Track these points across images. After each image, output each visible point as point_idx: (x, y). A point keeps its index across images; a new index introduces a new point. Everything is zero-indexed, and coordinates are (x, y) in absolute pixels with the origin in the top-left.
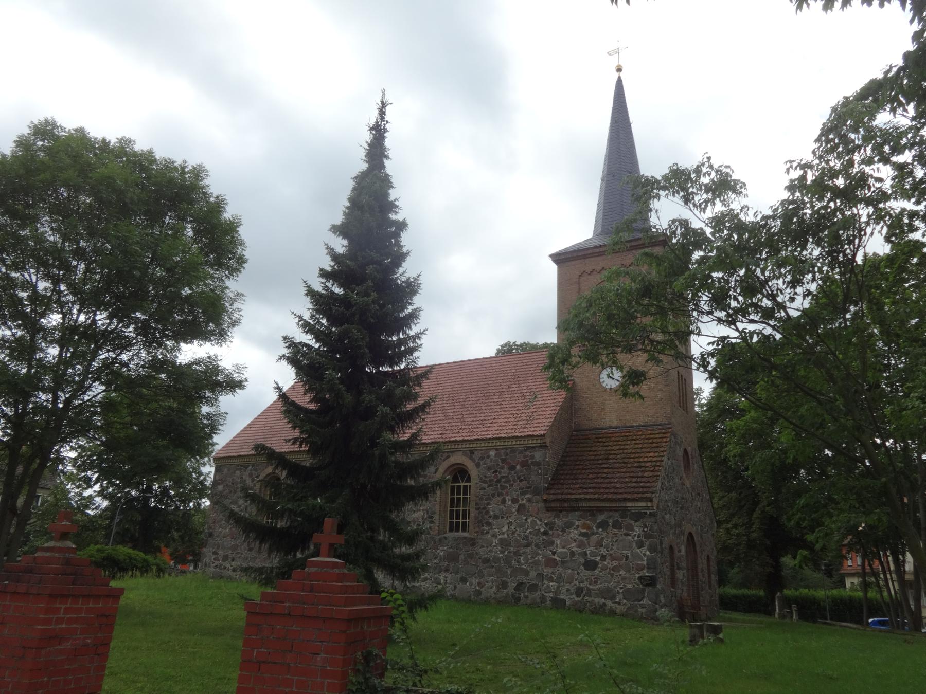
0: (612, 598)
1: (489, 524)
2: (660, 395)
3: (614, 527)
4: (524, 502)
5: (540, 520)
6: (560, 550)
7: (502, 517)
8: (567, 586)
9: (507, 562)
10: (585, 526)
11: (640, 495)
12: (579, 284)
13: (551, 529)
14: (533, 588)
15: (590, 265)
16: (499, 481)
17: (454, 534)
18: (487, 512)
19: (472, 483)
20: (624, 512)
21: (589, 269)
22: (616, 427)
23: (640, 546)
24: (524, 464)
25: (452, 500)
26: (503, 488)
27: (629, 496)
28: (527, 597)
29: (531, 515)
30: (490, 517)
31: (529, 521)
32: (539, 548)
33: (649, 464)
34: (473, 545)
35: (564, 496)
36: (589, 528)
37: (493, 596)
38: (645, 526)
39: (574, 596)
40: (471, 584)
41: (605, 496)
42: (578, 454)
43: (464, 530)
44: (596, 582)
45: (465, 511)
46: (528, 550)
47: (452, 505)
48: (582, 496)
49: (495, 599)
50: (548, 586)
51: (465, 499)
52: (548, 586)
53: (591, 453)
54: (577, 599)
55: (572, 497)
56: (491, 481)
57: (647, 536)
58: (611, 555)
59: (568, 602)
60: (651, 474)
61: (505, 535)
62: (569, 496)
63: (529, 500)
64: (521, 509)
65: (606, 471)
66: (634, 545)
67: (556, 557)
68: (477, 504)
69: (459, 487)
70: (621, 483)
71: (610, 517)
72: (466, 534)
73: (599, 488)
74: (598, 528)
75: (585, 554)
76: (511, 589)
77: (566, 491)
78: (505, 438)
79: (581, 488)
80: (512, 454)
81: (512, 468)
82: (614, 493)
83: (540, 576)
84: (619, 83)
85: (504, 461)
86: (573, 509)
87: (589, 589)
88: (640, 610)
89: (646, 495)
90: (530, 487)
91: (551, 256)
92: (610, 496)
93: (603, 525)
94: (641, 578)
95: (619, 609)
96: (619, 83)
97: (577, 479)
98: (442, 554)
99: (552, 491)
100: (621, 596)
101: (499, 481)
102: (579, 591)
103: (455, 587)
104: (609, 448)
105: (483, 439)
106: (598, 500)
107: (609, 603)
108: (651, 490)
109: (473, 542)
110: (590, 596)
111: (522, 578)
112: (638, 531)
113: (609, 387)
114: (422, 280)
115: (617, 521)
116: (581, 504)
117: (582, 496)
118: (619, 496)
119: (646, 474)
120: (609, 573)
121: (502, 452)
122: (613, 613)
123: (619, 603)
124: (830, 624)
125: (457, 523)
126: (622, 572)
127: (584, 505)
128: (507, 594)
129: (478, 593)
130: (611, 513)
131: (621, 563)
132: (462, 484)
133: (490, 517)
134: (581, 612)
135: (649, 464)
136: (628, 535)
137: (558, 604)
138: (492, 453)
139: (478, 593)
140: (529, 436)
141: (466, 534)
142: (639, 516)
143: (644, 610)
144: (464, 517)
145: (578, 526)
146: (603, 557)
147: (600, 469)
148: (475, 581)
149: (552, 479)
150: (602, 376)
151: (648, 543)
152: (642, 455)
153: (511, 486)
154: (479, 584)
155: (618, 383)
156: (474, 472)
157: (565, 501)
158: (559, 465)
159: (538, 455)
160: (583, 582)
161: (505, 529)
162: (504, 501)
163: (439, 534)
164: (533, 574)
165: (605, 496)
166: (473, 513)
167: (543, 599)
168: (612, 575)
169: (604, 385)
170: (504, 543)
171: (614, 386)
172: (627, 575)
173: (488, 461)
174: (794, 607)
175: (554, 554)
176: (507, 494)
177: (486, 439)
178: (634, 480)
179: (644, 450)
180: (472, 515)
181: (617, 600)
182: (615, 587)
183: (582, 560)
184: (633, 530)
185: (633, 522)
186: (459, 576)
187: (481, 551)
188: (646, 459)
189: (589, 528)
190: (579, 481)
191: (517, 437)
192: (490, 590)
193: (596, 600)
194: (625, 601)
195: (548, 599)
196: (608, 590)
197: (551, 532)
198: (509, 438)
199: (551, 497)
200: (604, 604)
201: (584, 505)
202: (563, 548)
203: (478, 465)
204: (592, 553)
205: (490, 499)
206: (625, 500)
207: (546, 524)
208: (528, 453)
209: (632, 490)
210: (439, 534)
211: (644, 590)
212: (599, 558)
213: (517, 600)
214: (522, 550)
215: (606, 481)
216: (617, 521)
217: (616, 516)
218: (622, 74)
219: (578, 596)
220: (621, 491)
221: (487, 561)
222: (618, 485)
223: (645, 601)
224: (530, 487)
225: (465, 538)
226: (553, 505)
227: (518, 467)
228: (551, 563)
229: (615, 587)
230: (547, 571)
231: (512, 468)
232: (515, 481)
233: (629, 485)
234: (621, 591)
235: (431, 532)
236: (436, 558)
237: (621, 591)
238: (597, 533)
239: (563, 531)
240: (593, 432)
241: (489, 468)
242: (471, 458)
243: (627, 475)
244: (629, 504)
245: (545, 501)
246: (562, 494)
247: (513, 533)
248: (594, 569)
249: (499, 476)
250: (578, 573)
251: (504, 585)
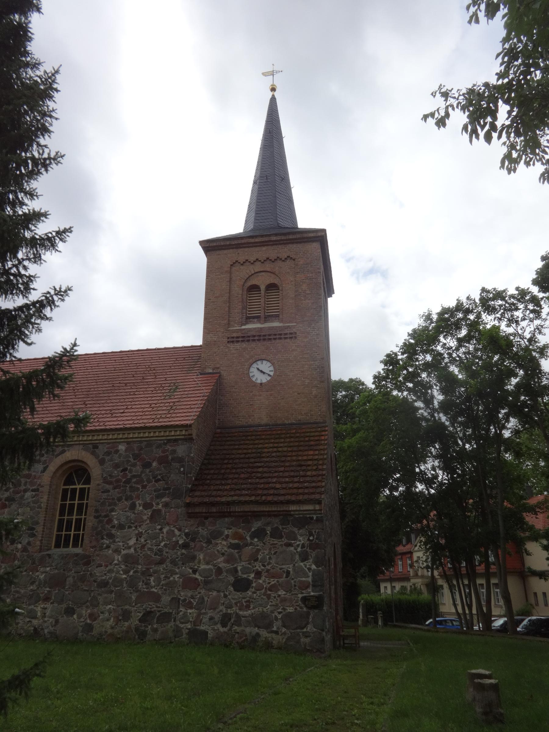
0: (268, 627)
1: (111, 536)
2: (314, 392)
3: (272, 536)
4: (160, 507)
5: (180, 530)
6: (203, 567)
7: (130, 527)
8: (211, 613)
9: (132, 584)
10: (236, 536)
11: (306, 497)
12: (230, 273)
13: (193, 540)
14: (165, 617)
15: (242, 255)
16: (128, 481)
17: (63, 550)
18: (110, 521)
19: (92, 486)
20: (286, 517)
21: (241, 259)
22: (266, 425)
23: (304, 558)
24: (163, 461)
25: (63, 507)
26: (133, 489)
27: (293, 498)
28: (155, 630)
29: (168, 524)
30: (113, 527)
31: (165, 530)
32: (175, 565)
33: (310, 463)
34: (88, 563)
35: (212, 499)
36: (241, 538)
37: (110, 631)
38: (311, 534)
39: (219, 626)
40: (80, 617)
41: (264, 498)
42: (225, 452)
43: (75, 545)
44: (248, 607)
45: (78, 521)
46: (161, 568)
47: (62, 513)
48: (235, 498)
49: (112, 635)
50: (185, 614)
51: (80, 506)
52: (185, 614)
53: (240, 451)
54: (222, 630)
55: (224, 499)
56: (118, 481)
57: (313, 546)
58: (268, 571)
59: (211, 635)
60: (314, 473)
61: (132, 550)
62: (218, 499)
63: (166, 505)
64: (155, 516)
65: (260, 470)
66: (297, 557)
67: (197, 576)
68: (97, 511)
69: (74, 491)
70: (280, 483)
71: (268, 524)
72: (78, 550)
73: (255, 489)
74: (252, 537)
75: (236, 570)
76: (134, 621)
77: (214, 493)
78: (141, 428)
79: (232, 489)
80: (149, 447)
81: (147, 465)
82: (274, 495)
83: (176, 601)
84: (273, 101)
85: (136, 457)
86: (223, 515)
87: (238, 616)
88: (303, 640)
89: (313, 497)
90: (168, 489)
91: (202, 243)
92: (270, 498)
93: (260, 534)
94: (304, 599)
95: (276, 640)
96: (273, 101)
97: (226, 479)
98: (42, 577)
99: (198, 493)
100: (279, 623)
101: (128, 481)
102: (225, 620)
103: (57, 622)
104: (260, 446)
105: (111, 430)
106: (257, 503)
107: (264, 633)
108: (319, 490)
109: (87, 560)
110: (239, 625)
111: (151, 606)
112: (302, 540)
113: (259, 381)
114: (61, 82)
115: (277, 528)
116: (233, 509)
117: (235, 498)
118: (281, 498)
119: (309, 473)
120: (265, 594)
121: (135, 446)
122: (268, 646)
123: (276, 633)
124: (395, 626)
125: (67, 537)
126: (282, 592)
127: (238, 509)
128: (129, 627)
129: (89, 628)
130: (269, 519)
131: (281, 580)
132: (78, 487)
133: (113, 527)
134: (226, 646)
135: (310, 463)
136: (290, 545)
137: (198, 637)
138: (122, 447)
139: (89, 628)
140: (172, 426)
141: (78, 550)
142: (303, 522)
143: (307, 640)
144: (78, 528)
145: (227, 536)
146: (258, 574)
147: (253, 467)
148: (85, 612)
149: (196, 479)
150: (252, 370)
151: (314, 554)
152: (300, 453)
153: (144, 487)
154: (91, 616)
155: (269, 378)
156: (96, 471)
157: (213, 504)
158: (203, 464)
159: (181, 450)
160: (231, 607)
161: (132, 542)
162: (133, 507)
163: (40, 550)
164: (166, 599)
165: (264, 498)
166: (90, 521)
167: (177, 631)
168: (269, 597)
169: (254, 379)
170: (130, 561)
171: (264, 381)
172: (288, 596)
173: (116, 456)
174: (380, 614)
175: (195, 572)
176: (138, 498)
177: (116, 430)
178: (296, 479)
179: (301, 448)
180: (89, 524)
181: (275, 629)
182: (272, 612)
183: (232, 579)
184: (295, 539)
185: (295, 530)
186: (64, 606)
187: (97, 572)
188: (305, 458)
189: (241, 538)
190: (230, 481)
191: (156, 427)
192: (106, 624)
193: (248, 630)
194: (284, 630)
195: (185, 632)
196: (263, 616)
197: (192, 544)
198: (145, 428)
199: (196, 500)
200: (258, 635)
201: (238, 509)
202: (207, 563)
203: (102, 462)
204: (246, 570)
205: (115, 505)
206: (289, 502)
207: (187, 535)
208: (169, 447)
209: (295, 491)
210: (40, 550)
211: (308, 614)
212: (252, 575)
213: (142, 635)
214: (154, 568)
215: (262, 481)
216: (277, 528)
217: (276, 522)
218: (276, 94)
219: (224, 626)
220: (282, 492)
221: (104, 584)
222: (278, 486)
223: (310, 628)
224: (168, 489)
225: (77, 555)
226: (197, 510)
227: (154, 464)
228: (190, 583)
229: (272, 612)
230: (185, 594)
231: (147, 465)
232: (149, 481)
233: (291, 485)
234: (280, 616)
235: (30, 548)
236: (32, 583)
237: (280, 616)
238: (251, 544)
239: (209, 542)
240: (241, 430)
241: (116, 466)
242: (93, 453)
243: (287, 474)
244: (292, 508)
245: (188, 505)
246: (210, 496)
247: (143, 546)
248: (246, 589)
249: (129, 475)
250: (225, 596)
251: (126, 615)
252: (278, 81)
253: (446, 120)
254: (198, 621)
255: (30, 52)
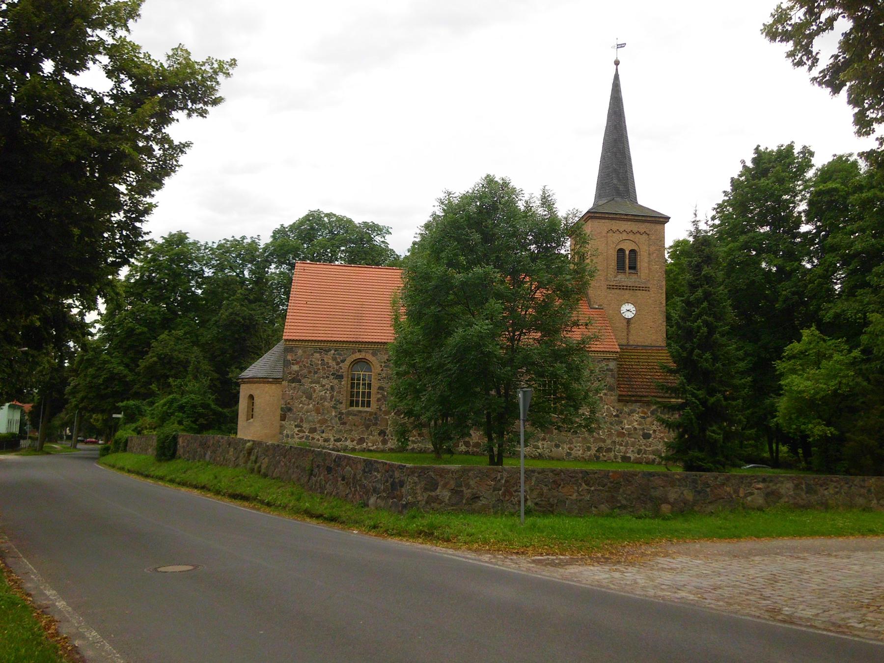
8: (632, 448)
10: (643, 412)
12: (607, 237)
14: (609, 450)
40: (563, 449)
59: (632, 458)
63: (605, 394)
83: (614, 442)
84: (617, 77)
86: (636, 401)
96: (617, 77)
148: (566, 447)
164: (609, 441)
189: (646, 413)
193: (650, 456)
228: (621, 434)
245: (620, 395)
252: (622, 54)
253: (262, 245)
254: (626, 452)
255: (223, 242)
